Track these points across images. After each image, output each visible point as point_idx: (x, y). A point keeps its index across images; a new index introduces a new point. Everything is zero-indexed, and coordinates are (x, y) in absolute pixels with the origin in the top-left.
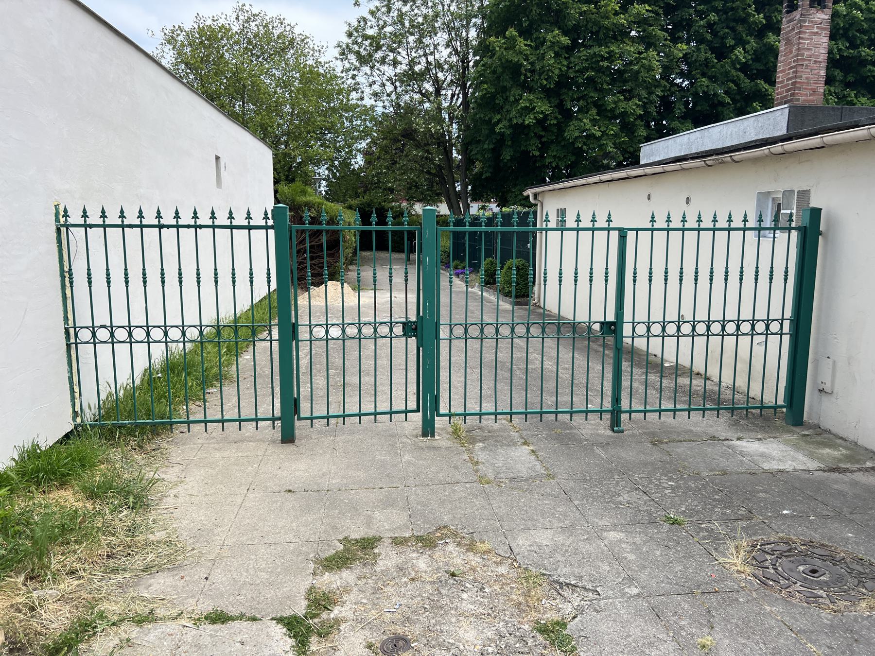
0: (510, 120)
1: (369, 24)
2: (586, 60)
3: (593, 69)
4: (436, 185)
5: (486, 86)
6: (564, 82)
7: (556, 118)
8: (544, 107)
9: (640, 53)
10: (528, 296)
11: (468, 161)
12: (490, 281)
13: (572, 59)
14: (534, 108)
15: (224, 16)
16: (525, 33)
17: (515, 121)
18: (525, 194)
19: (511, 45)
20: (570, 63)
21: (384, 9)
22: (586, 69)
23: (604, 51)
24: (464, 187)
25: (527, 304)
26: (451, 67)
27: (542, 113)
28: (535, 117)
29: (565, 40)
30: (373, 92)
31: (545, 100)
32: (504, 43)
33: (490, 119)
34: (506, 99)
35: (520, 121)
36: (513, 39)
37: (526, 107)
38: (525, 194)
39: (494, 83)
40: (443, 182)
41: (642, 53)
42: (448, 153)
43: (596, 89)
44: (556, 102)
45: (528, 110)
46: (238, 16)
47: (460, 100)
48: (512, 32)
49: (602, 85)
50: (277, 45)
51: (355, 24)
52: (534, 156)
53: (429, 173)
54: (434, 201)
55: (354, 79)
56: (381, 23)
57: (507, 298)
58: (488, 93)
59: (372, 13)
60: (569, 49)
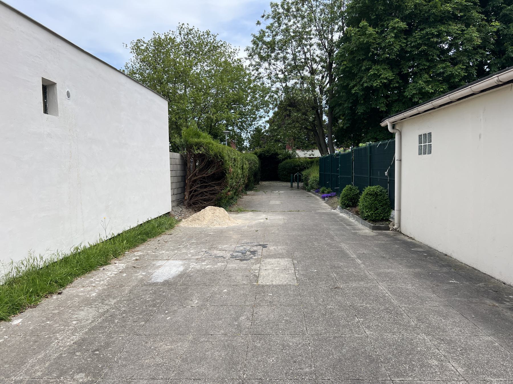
0: (362, 85)
1: (267, 34)
2: (420, 39)
3: (425, 45)
4: (313, 136)
5: (345, 63)
6: (403, 55)
7: (398, 82)
8: (388, 74)
9: (463, 31)
10: (387, 220)
11: (333, 119)
12: (350, 204)
13: (409, 39)
14: (380, 75)
15: (171, 32)
16: (374, 24)
17: (365, 85)
18: (383, 124)
19: (363, 32)
20: (408, 41)
21: (276, 24)
22: (420, 45)
23: (434, 31)
24: (331, 140)
25: (388, 229)
26: (322, 60)
27: (386, 78)
28: (381, 82)
29: (403, 25)
30: (270, 76)
31: (388, 70)
32: (359, 31)
33: (348, 85)
34: (360, 70)
35: (369, 85)
36: (364, 28)
37: (375, 74)
38: (383, 124)
39: (352, 60)
40: (316, 134)
41: (464, 30)
42: (319, 117)
43: (428, 60)
44: (397, 71)
45: (376, 76)
46: (180, 32)
47: (327, 81)
48: (364, 23)
49: (433, 56)
50: (204, 47)
51: (258, 35)
52: (382, 111)
53: (306, 128)
54: (313, 149)
55: (257, 70)
56: (274, 33)
57: (366, 222)
58: (347, 67)
59: (268, 28)
60: (408, 32)
